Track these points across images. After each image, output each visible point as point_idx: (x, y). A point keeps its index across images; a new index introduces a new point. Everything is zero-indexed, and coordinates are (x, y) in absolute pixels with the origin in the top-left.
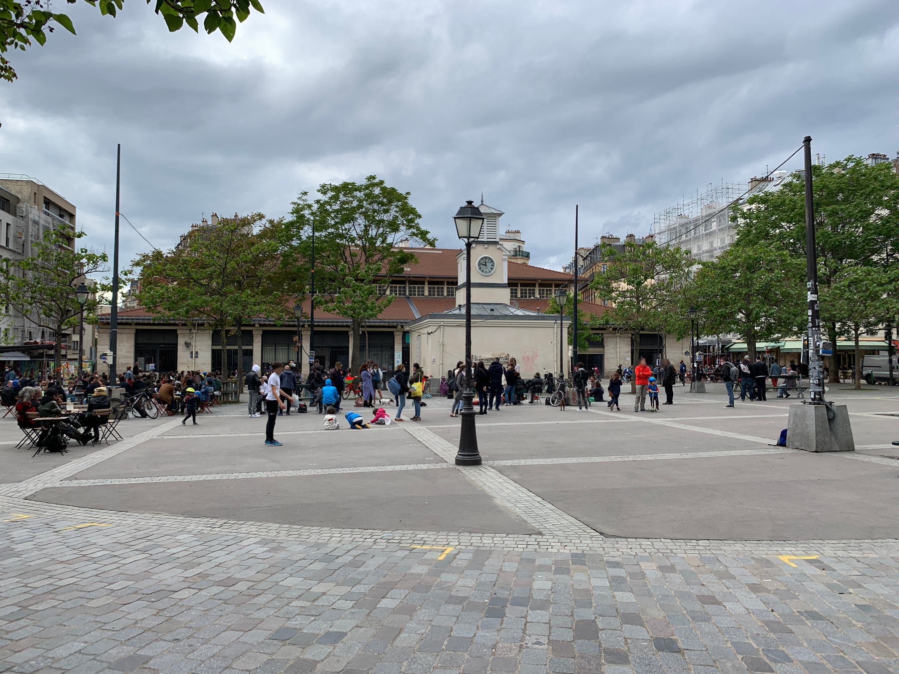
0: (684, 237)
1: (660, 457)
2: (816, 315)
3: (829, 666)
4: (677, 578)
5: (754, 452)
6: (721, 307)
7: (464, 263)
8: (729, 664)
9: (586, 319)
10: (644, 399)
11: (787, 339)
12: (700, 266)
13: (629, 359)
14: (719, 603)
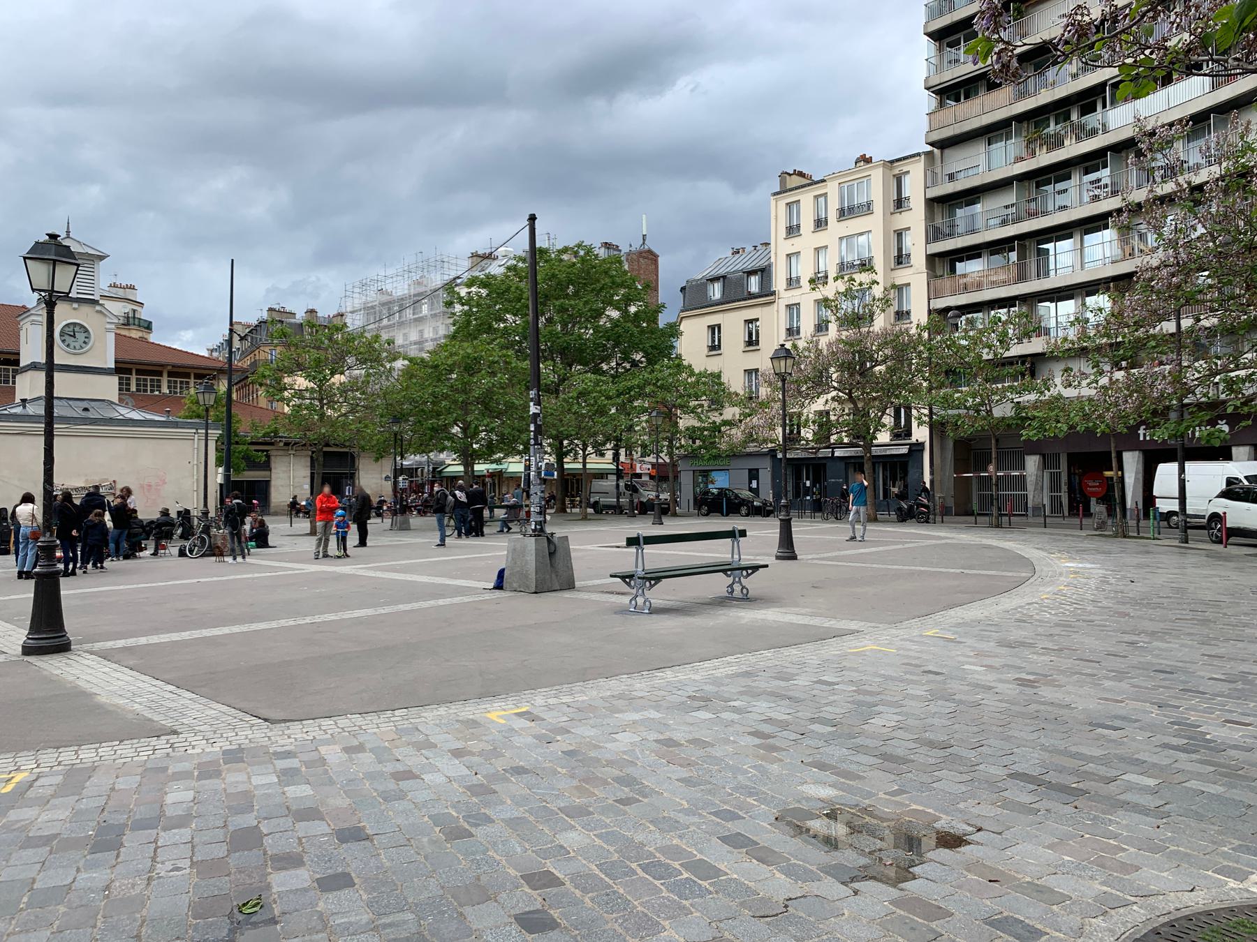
0: (385, 322)
1: (347, 615)
2: (538, 431)
3: (532, 818)
4: (366, 758)
5: (466, 599)
6: (432, 417)
7: (42, 331)
8: (425, 840)
9: (244, 427)
10: (327, 540)
11: (510, 460)
12: (406, 362)
13: (307, 487)
14: (417, 777)
